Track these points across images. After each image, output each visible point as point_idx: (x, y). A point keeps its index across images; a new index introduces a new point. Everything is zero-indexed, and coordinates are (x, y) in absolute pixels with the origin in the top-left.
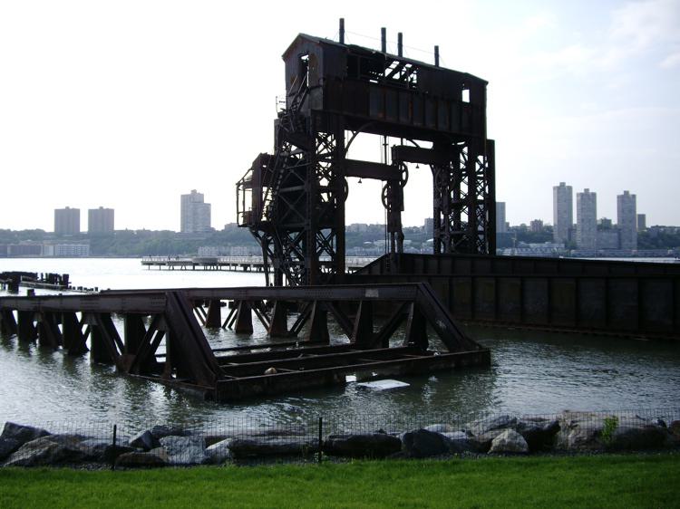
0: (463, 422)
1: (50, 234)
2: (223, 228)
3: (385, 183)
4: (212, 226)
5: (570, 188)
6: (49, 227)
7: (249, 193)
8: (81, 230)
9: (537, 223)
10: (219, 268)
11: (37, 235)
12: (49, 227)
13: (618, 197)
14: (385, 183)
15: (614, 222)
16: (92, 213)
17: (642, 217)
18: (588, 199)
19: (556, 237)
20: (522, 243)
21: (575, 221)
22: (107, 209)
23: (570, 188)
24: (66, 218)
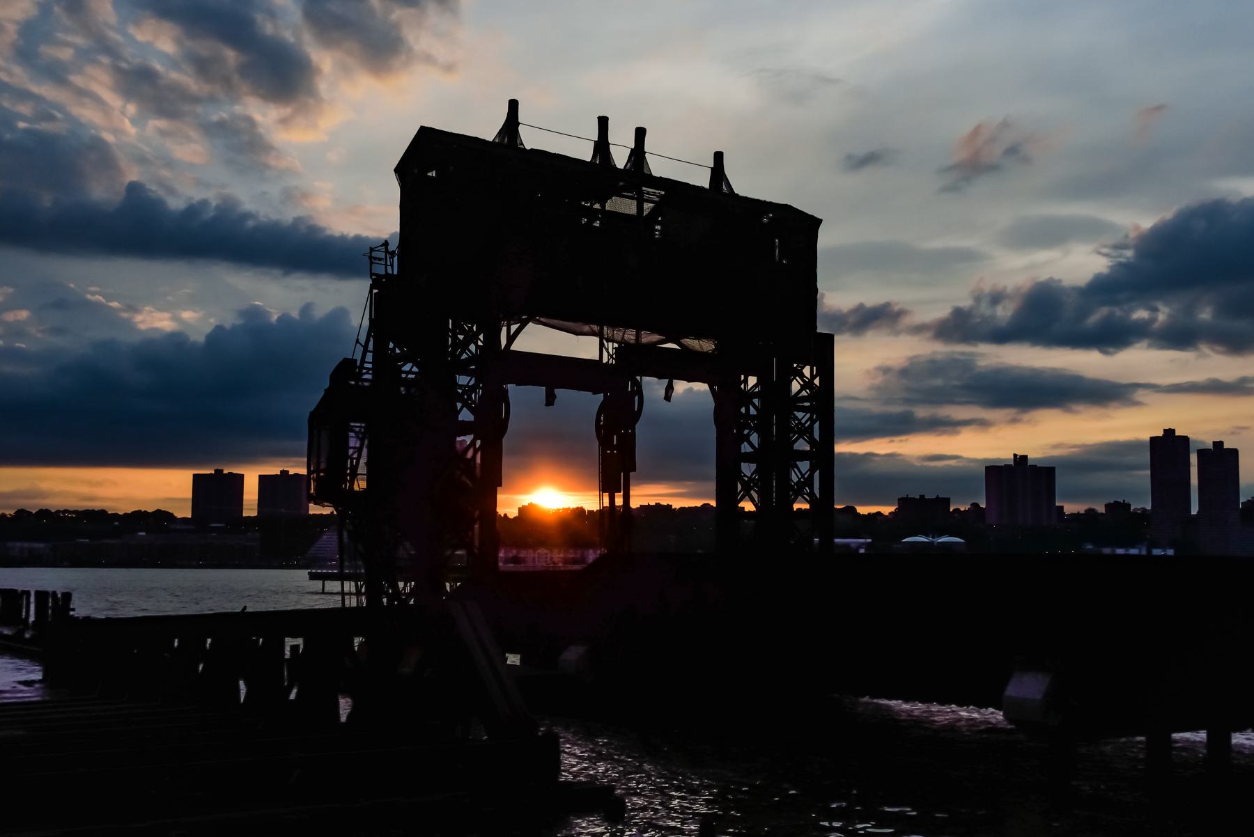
3: (601, 397)
14: (601, 397)
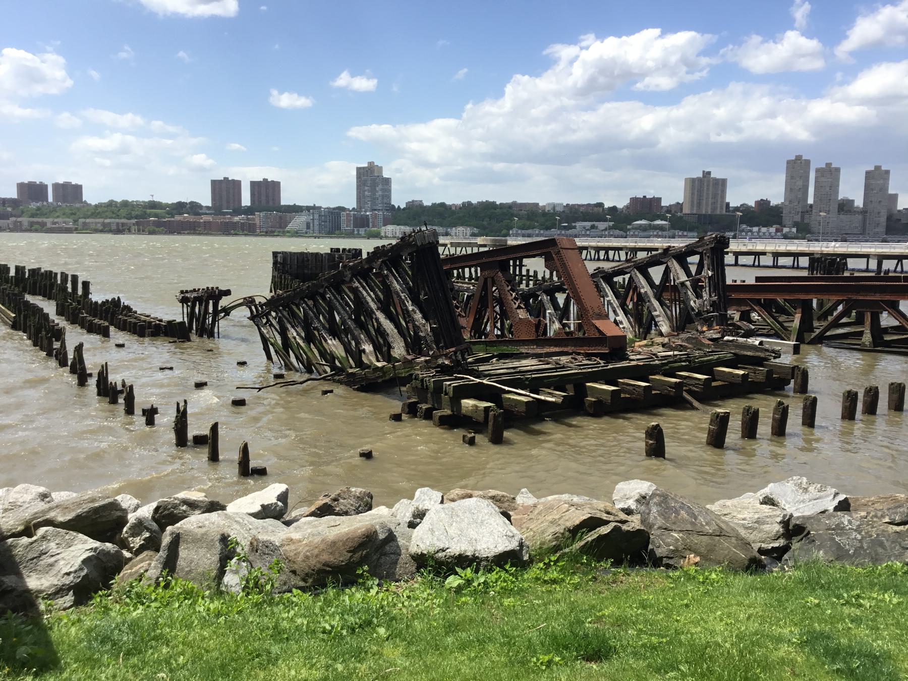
0: (651, 635)
1: (208, 208)
2: (403, 206)
4: (393, 203)
5: (808, 162)
6: (206, 200)
7: (775, 192)
8: (243, 205)
9: (763, 204)
10: (873, 264)
11: (194, 208)
12: (206, 200)
13: (788, 162)
15: (859, 203)
16: (254, 184)
17: (895, 197)
18: (830, 175)
19: (787, 220)
20: (744, 226)
21: (810, 201)
22: (233, 180)
23: (808, 162)
24: (225, 190)
